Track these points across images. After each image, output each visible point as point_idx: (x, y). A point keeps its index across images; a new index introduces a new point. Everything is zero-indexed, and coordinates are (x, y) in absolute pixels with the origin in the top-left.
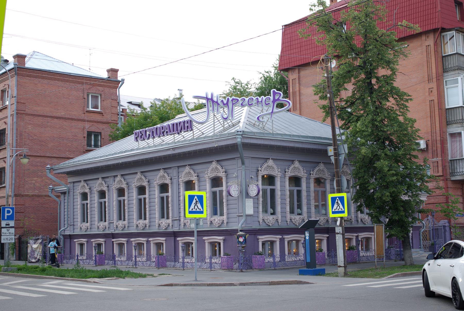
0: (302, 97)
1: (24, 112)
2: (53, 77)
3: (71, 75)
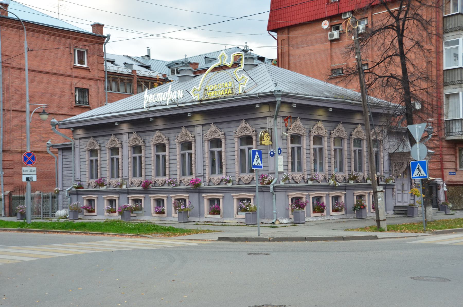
0: (291, 58)
2: (38, 29)
3: (57, 28)
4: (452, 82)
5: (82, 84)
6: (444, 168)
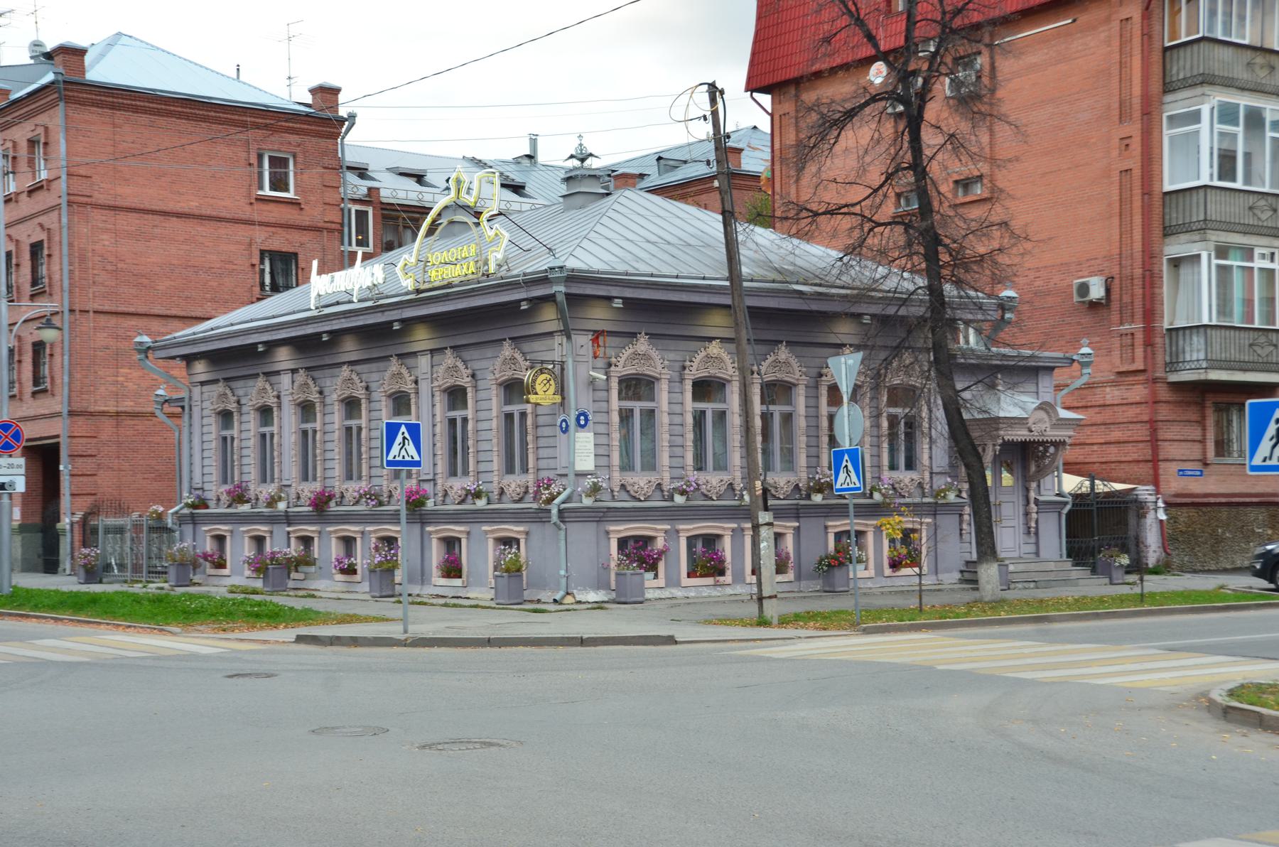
1: (88, 200)
4: (1184, 224)
5: (279, 242)
6: (1161, 457)
